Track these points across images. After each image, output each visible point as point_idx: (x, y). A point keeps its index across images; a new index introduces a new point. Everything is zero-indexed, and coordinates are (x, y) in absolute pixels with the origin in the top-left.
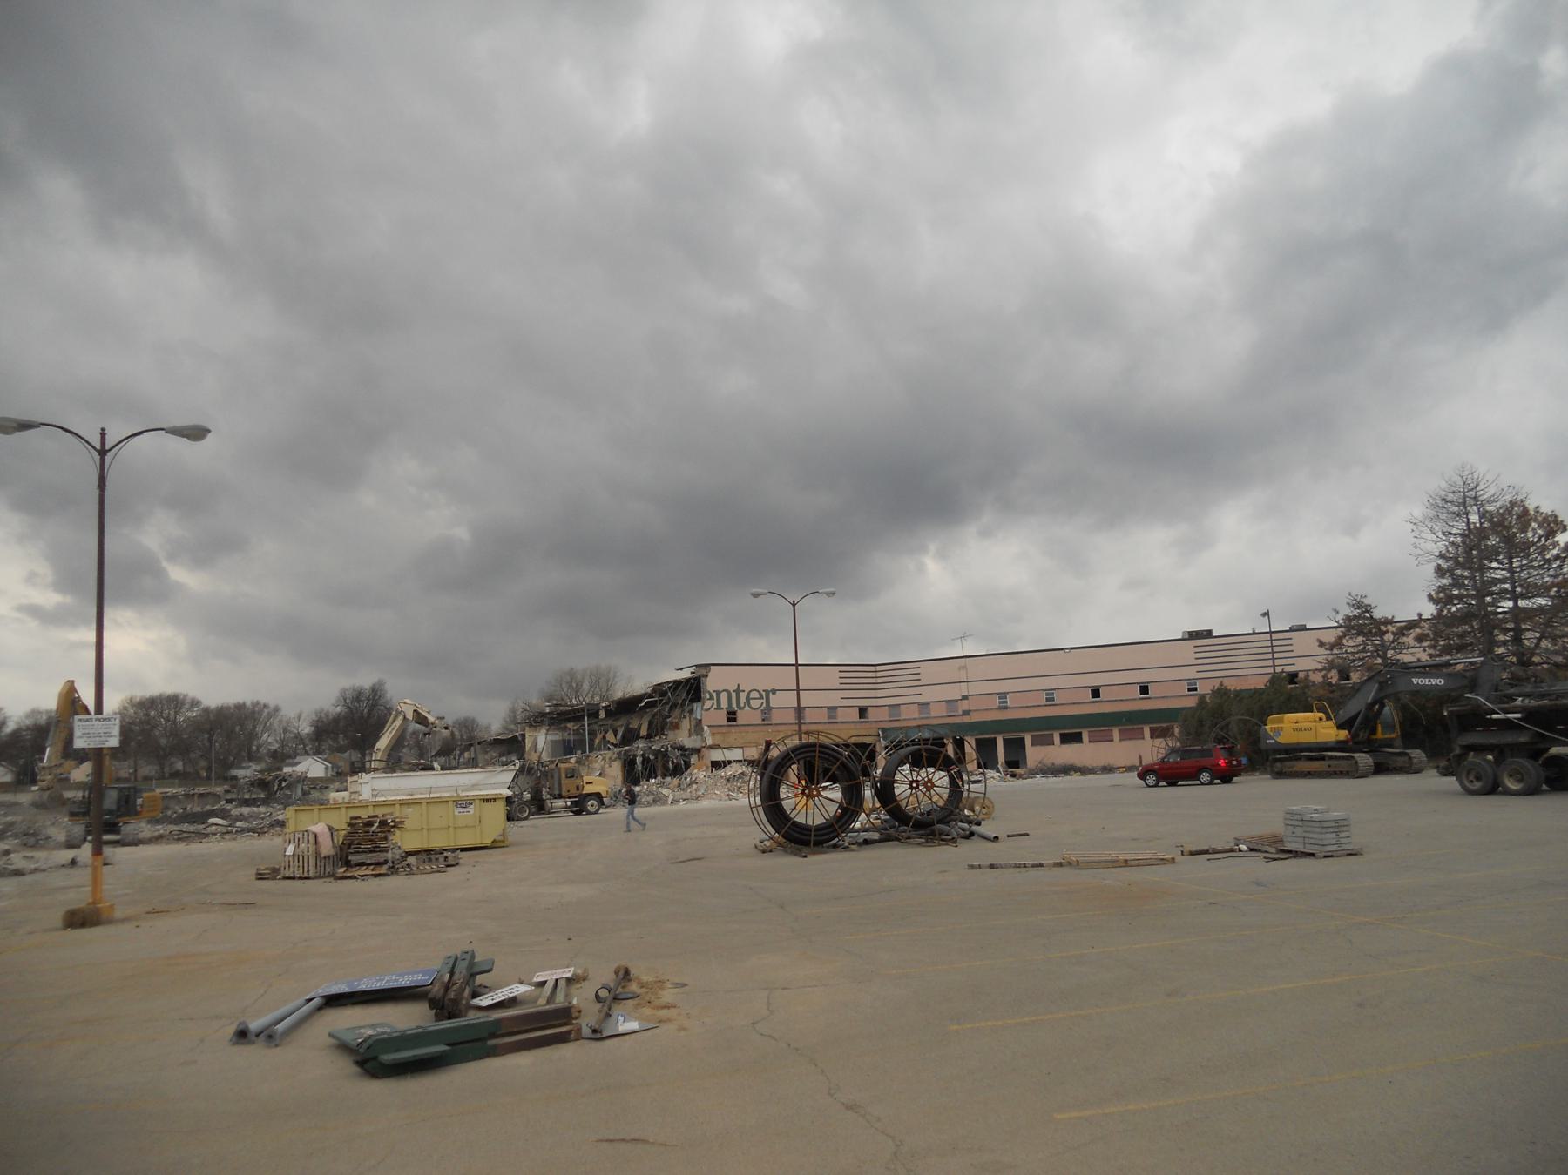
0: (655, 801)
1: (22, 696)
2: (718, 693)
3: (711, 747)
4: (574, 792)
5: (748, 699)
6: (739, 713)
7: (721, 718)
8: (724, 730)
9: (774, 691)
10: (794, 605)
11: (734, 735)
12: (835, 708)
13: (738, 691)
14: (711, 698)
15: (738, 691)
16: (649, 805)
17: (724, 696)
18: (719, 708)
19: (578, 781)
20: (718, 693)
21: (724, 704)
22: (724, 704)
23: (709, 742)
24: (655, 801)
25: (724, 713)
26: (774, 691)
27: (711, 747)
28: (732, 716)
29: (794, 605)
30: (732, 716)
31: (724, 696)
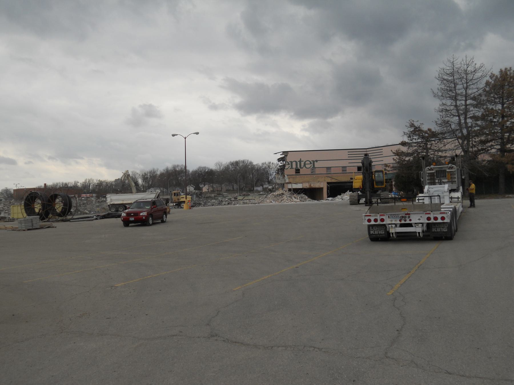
0: (228, 204)
1: (512, 144)
2: (292, 162)
3: (288, 183)
4: (177, 201)
5: (305, 164)
6: (301, 170)
7: (293, 172)
8: (294, 176)
9: (317, 161)
10: (185, 138)
11: (298, 178)
12: (346, 167)
13: (300, 161)
14: (289, 164)
15: (300, 161)
16: (210, 206)
17: (294, 164)
18: (292, 168)
19: (178, 197)
20: (292, 162)
21: (294, 166)
22: (294, 166)
23: (287, 181)
24: (228, 204)
25: (294, 170)
26: (317, 161)
27: (288, 183)
28: (298, 171)
29: (185, 138)
30: (298, 171)
31: (294, 164)
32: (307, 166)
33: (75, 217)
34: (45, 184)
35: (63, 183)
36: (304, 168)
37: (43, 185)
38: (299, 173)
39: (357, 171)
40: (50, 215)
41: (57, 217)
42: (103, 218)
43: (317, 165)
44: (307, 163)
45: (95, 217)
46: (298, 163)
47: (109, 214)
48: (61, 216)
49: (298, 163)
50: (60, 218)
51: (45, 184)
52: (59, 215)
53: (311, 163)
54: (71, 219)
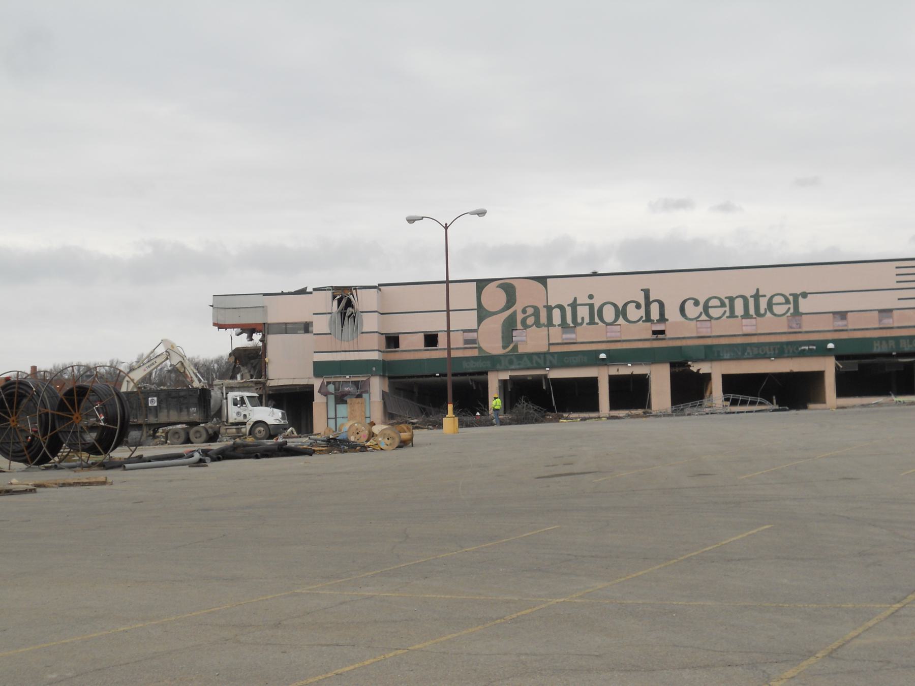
9: (805, 295)
10: (446, 227)
13: (757, 297)
15: (757, 297)
20: (732, 300)
26: (805, 295)
29: (446, 227)
32: (778, 310)
33: (147, 451)
34: (34, 368)
35: (79, 366)
36: (768, 314)
37: (29, 371)
38: (397, 345)
39: (423, 347)
40: (65, 450)
41: (85, 455)
42: (219, 459)
43: (805, 305)
44: (775, 300)
45: (197, 456)
46: (569, 311)
47: (235, 447)
48: (99, 453)
49: (569, 311)
50: (94, 458)
51: (34, 368)
52: (92, 450)
53: (723, 305)
54: (129, 460)
